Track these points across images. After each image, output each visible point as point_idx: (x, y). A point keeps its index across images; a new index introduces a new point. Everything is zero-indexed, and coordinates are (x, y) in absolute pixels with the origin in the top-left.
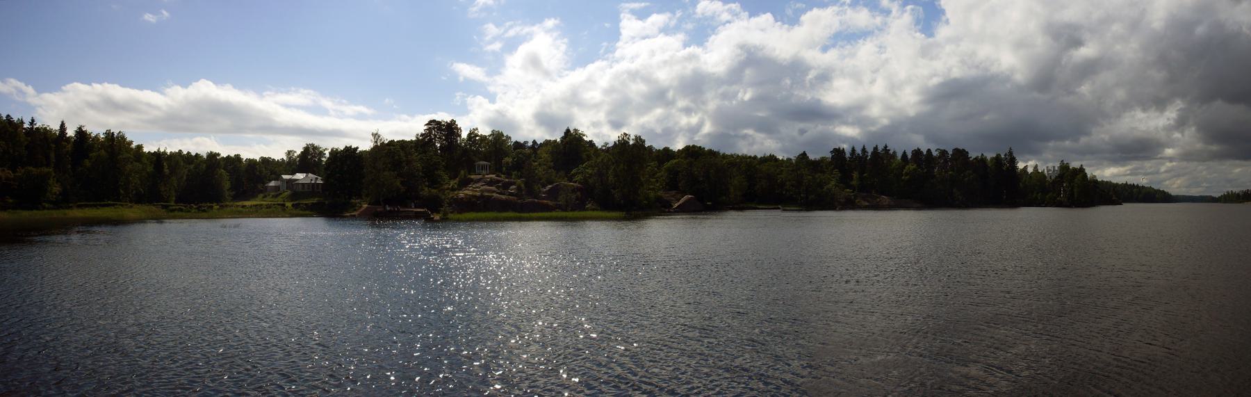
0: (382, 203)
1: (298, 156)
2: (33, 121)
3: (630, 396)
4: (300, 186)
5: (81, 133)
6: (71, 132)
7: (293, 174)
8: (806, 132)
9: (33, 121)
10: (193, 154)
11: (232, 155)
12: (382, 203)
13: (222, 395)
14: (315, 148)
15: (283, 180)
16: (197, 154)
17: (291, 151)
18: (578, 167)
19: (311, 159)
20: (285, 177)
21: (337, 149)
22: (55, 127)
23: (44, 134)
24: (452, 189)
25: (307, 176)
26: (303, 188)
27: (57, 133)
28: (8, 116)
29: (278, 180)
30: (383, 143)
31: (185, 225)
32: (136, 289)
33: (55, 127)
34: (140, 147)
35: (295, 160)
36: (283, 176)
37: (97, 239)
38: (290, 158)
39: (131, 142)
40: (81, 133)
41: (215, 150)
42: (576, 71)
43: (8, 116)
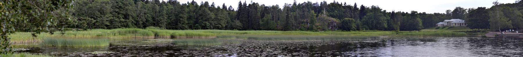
0: (500, 31)
1: (452, 12)
2: (345, 3)
3: (136, 56)
5: (363, 7)
6: (359, 7)
8: (32, 34)
9: (345, 3)
10: (405, 13)
13: (74, 54)
21: (472, 9)
22: (353, 5)
23: (349, 7)
24: (222, 29)
26: (458, 25)
27: (353, 7)
28: (337, 2)
30: (497, 5)
32: (68, 34)
33: (353, 5)
34: (385, 11)
35: (450, 14)
39: (381, 10)
40: (363, 7)
43: (337, 2)
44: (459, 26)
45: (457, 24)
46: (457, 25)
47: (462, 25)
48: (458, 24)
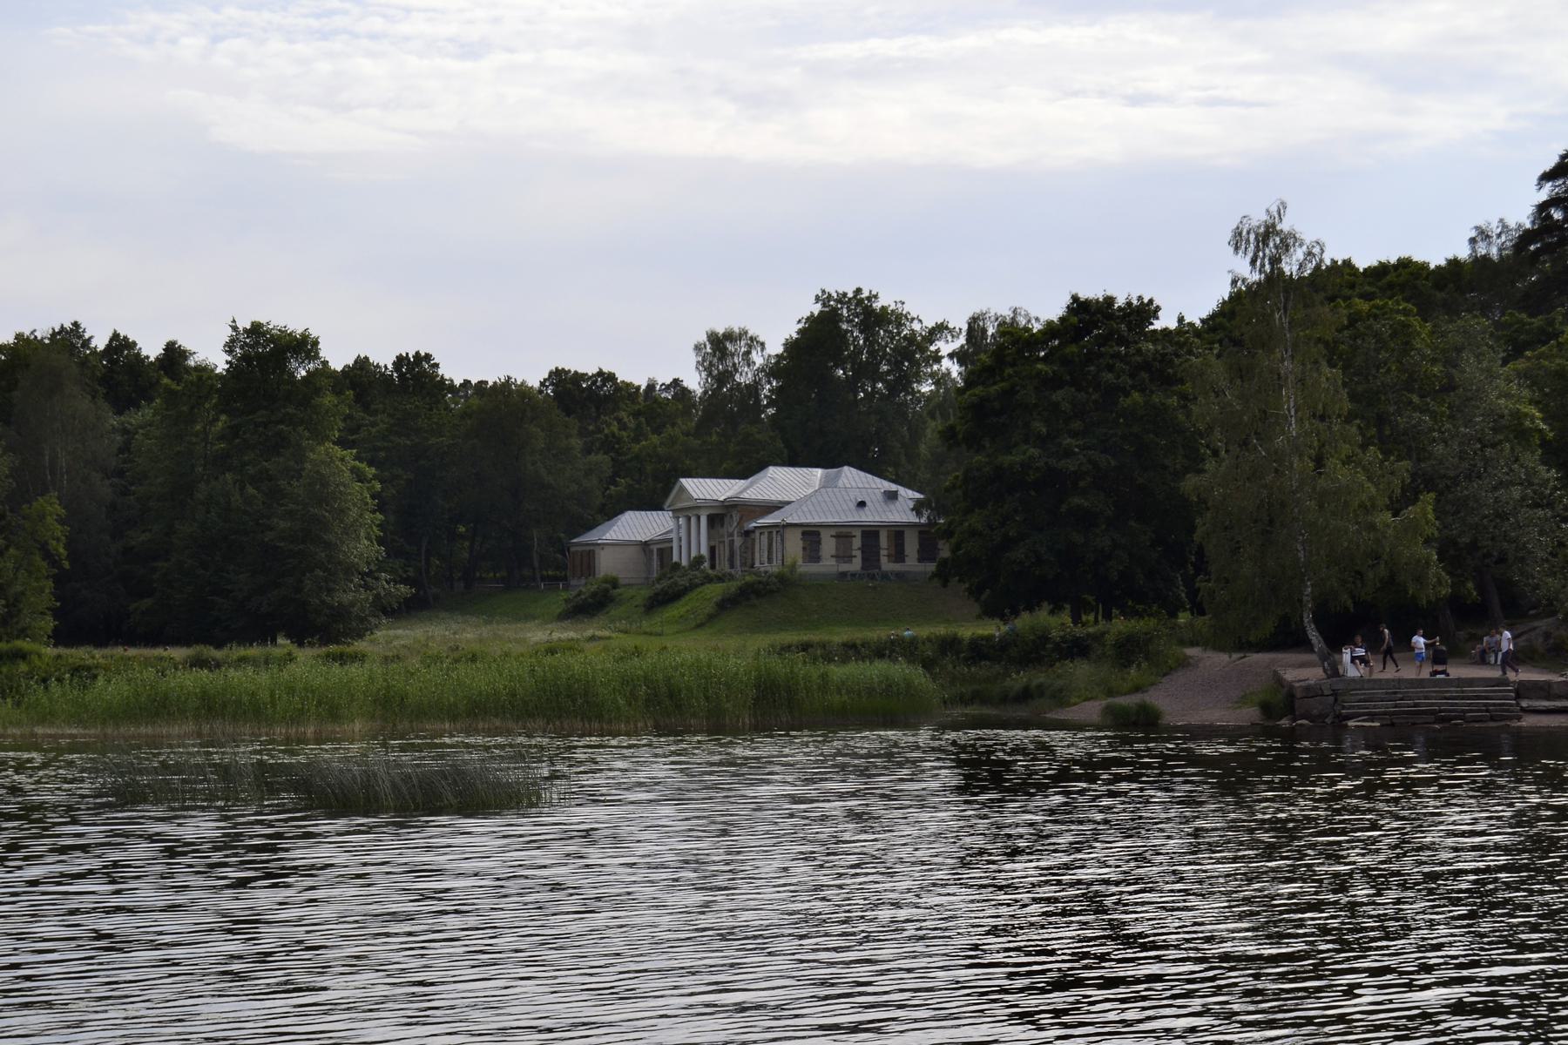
1: (775, 369)
4: (794, 546)
7: (746, 470)
10: (151, 349)
11: (384, 358)
12: (1314, 636)
14: (873, 317)
15: (688, 511)
16: (253, 323)
17: (730, 336)
18: (1451, 587)
19: (851, 385)
20: (705, 489)
25: (826, 484)
29: (658, 507)
31: (688, 657)
35: (754, 388)
36: (688, 483)
37: (701, 592)
38: (723, 378)
41: (286, 317)
42: (1086, 297)
44: (856, 565)
45: (828, 545)
46: (828, 563)
47: (886, 565)
48: (843, 533)
